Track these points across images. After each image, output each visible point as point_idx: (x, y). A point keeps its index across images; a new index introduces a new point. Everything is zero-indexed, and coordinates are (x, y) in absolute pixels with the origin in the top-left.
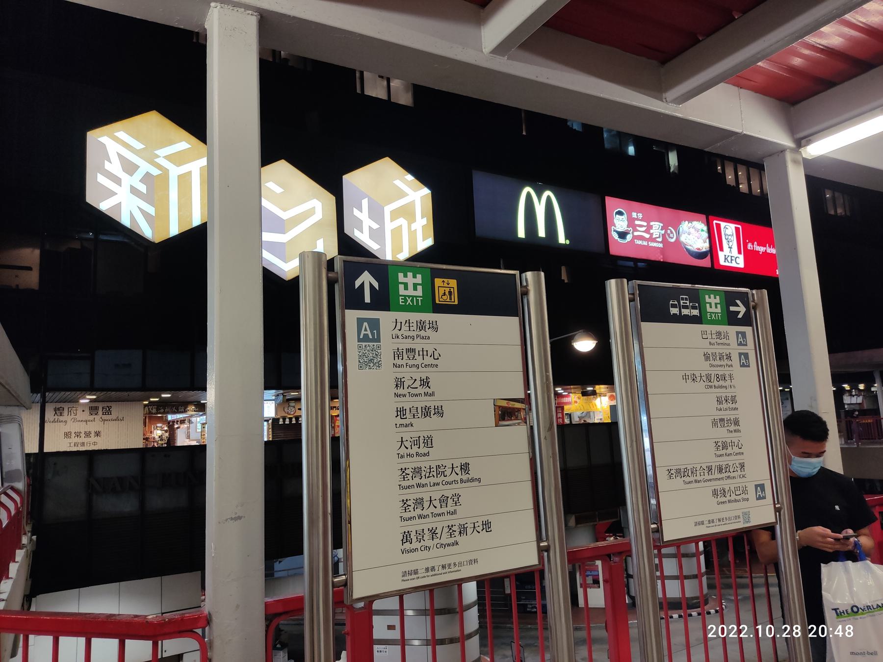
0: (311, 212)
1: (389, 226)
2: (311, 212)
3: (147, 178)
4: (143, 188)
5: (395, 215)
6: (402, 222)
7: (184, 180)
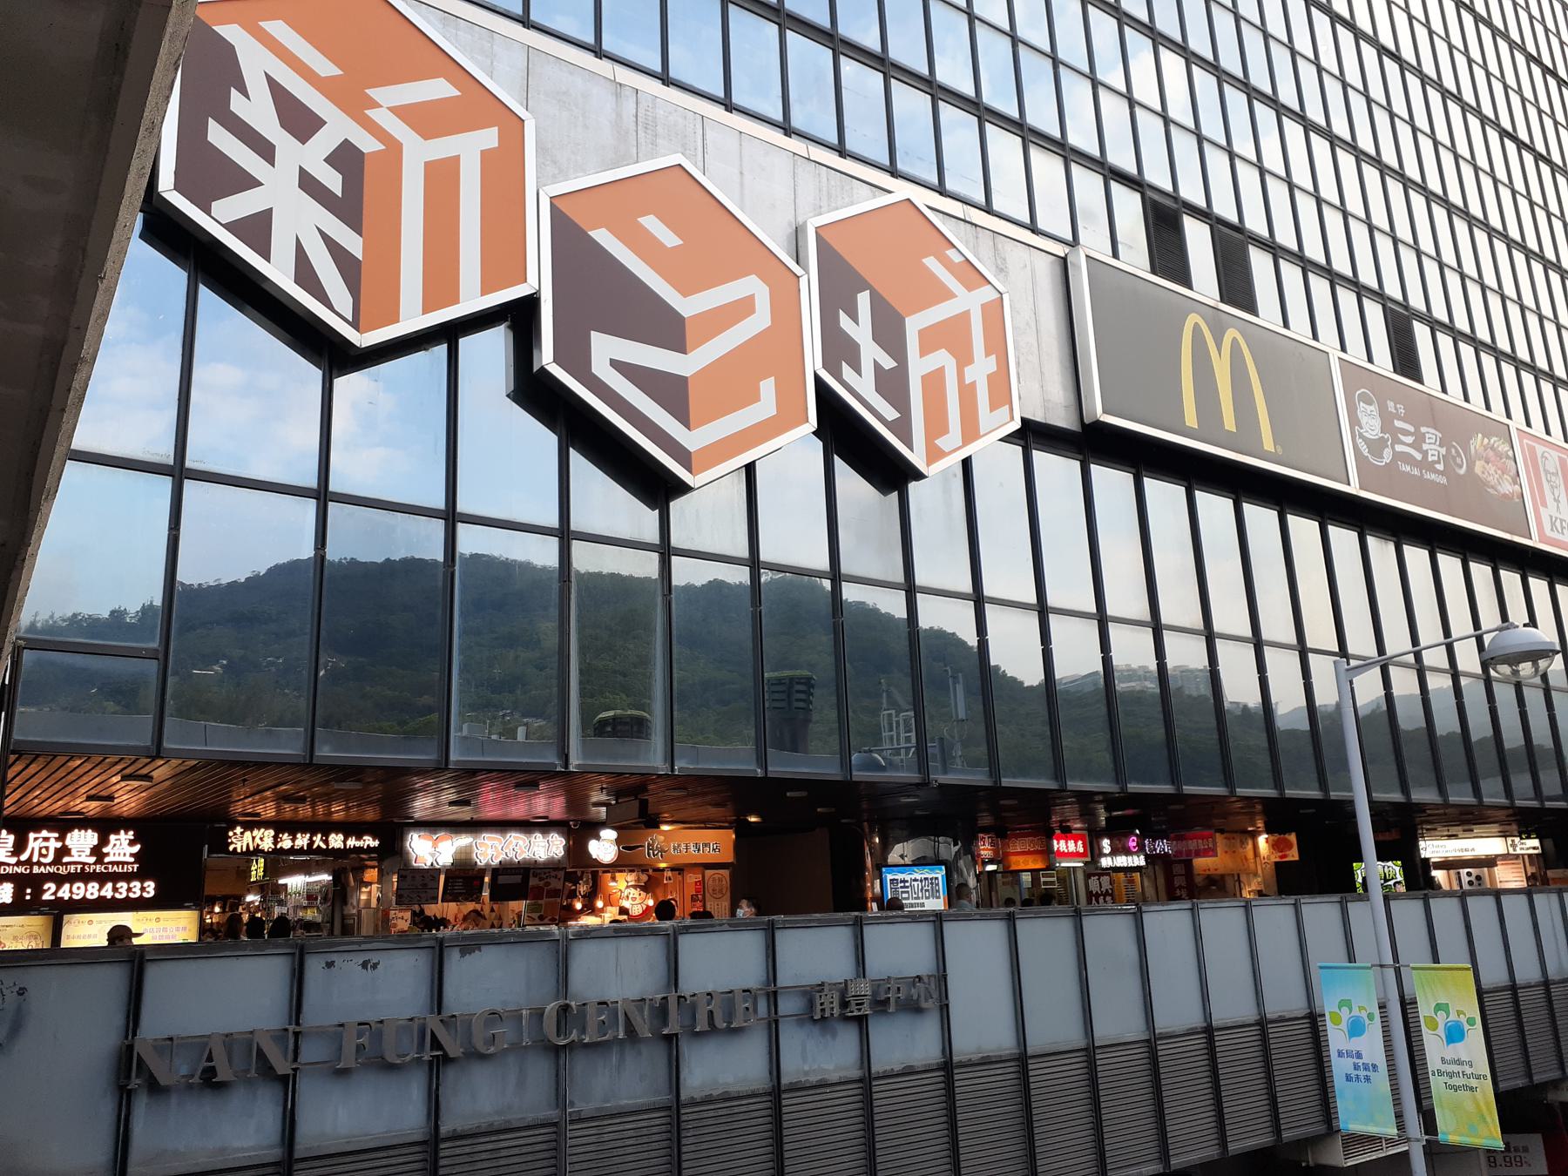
0: (745, 307)
1: (918, 367)
2: (745, 307)
3: (345, 158)
4: (333, 181)
5: (929, 341)
6: (942, 359)
7: (442, 177)
